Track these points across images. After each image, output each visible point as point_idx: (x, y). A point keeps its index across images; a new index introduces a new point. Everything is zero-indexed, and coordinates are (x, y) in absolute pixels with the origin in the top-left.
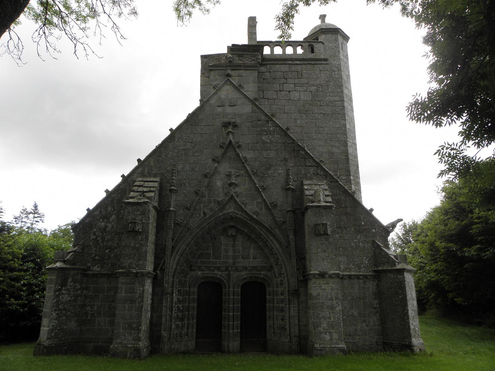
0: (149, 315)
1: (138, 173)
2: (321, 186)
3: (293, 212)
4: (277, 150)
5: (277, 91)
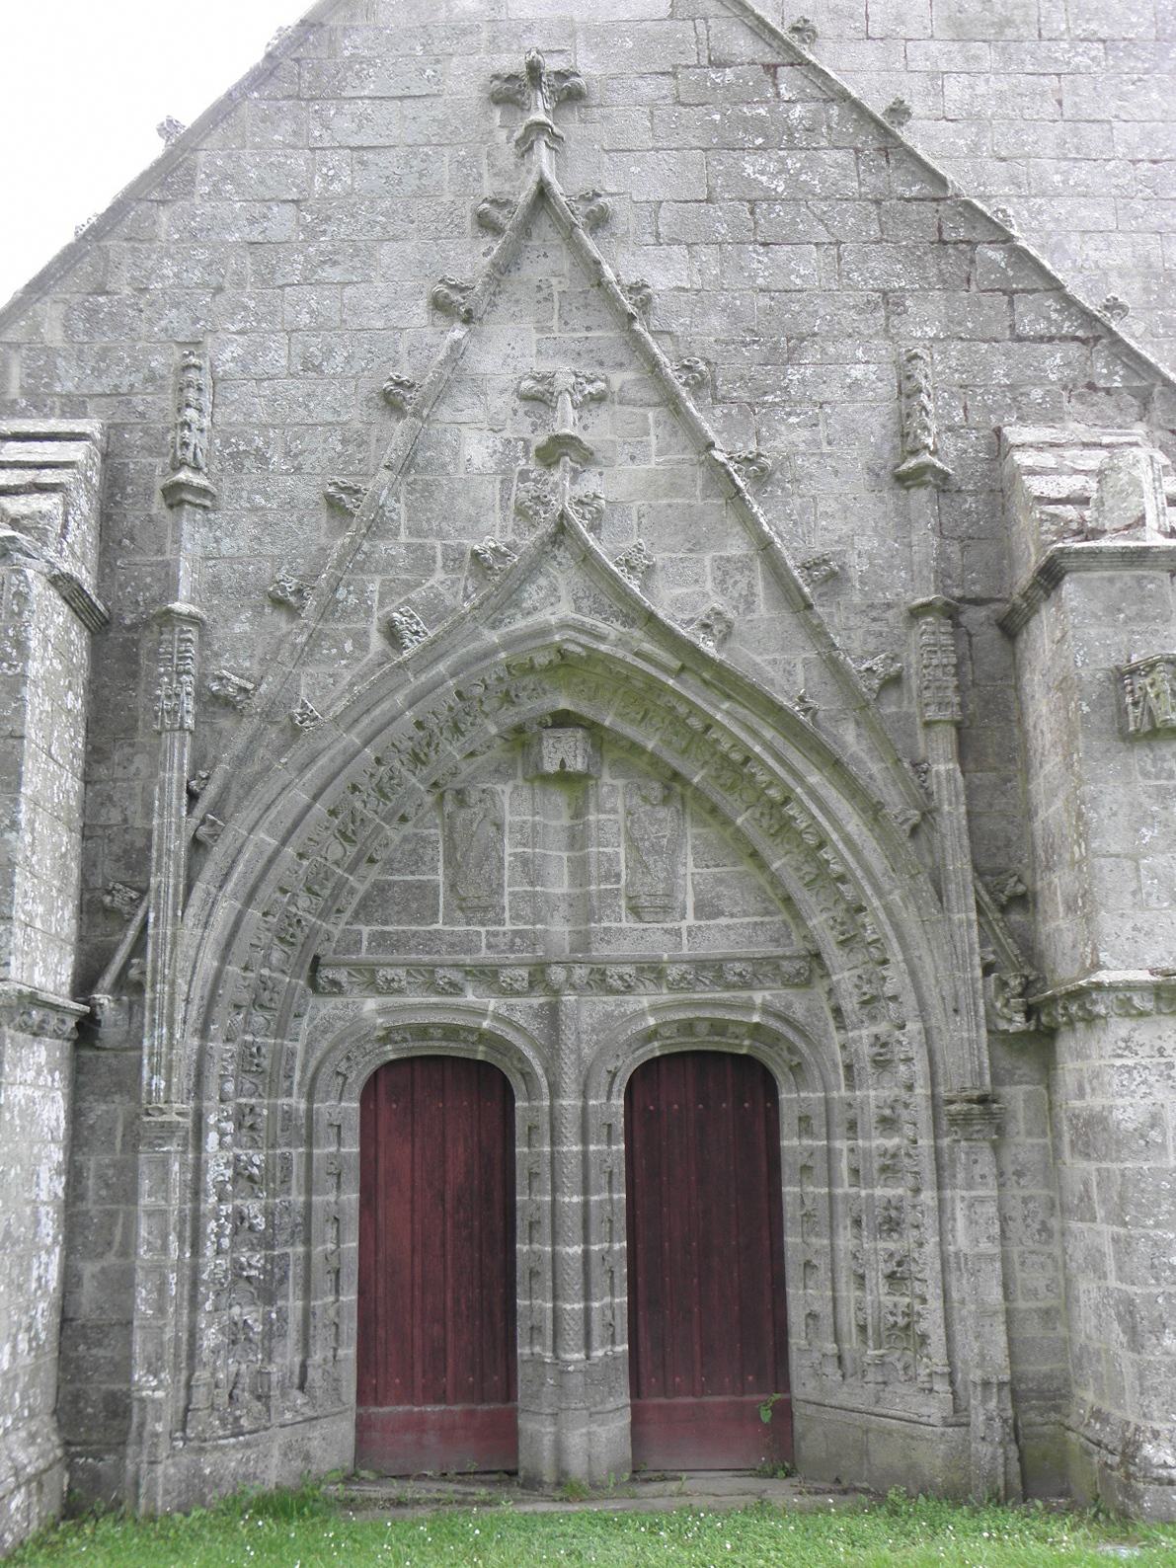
4: (838, 243)
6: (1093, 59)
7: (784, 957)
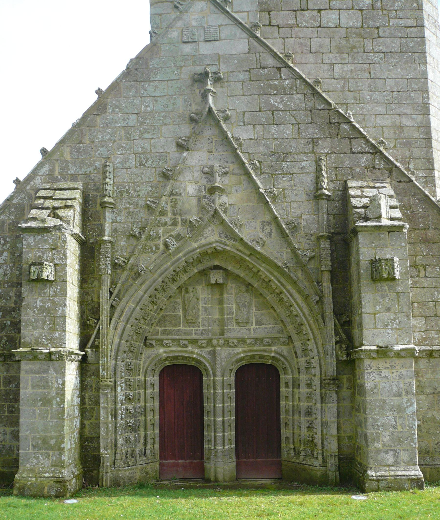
0: (77, 423)
1: (42, 175)
2: (381, 190)
3: (330, 238)
4: (299, 124)
5: (295, 11)
6: (380, 59)
7: (281, 337)
